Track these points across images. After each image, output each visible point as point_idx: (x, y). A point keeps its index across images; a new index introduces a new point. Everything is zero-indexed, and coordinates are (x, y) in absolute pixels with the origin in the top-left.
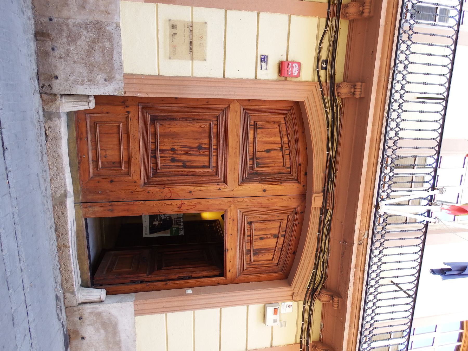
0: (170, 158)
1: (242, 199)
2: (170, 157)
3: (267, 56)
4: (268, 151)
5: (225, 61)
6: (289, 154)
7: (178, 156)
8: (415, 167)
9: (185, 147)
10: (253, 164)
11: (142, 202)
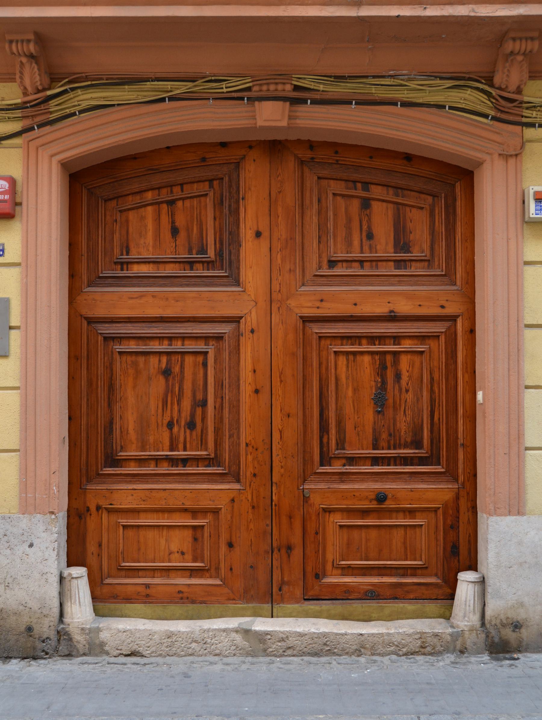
0: (188, 431)
1: (274, 282)
2: (185, 432)
4: (175, 231)
6: (182, 185)
7: (183, 415)
9: (165, 403)
10: (203, 262)
11: (274, 488)
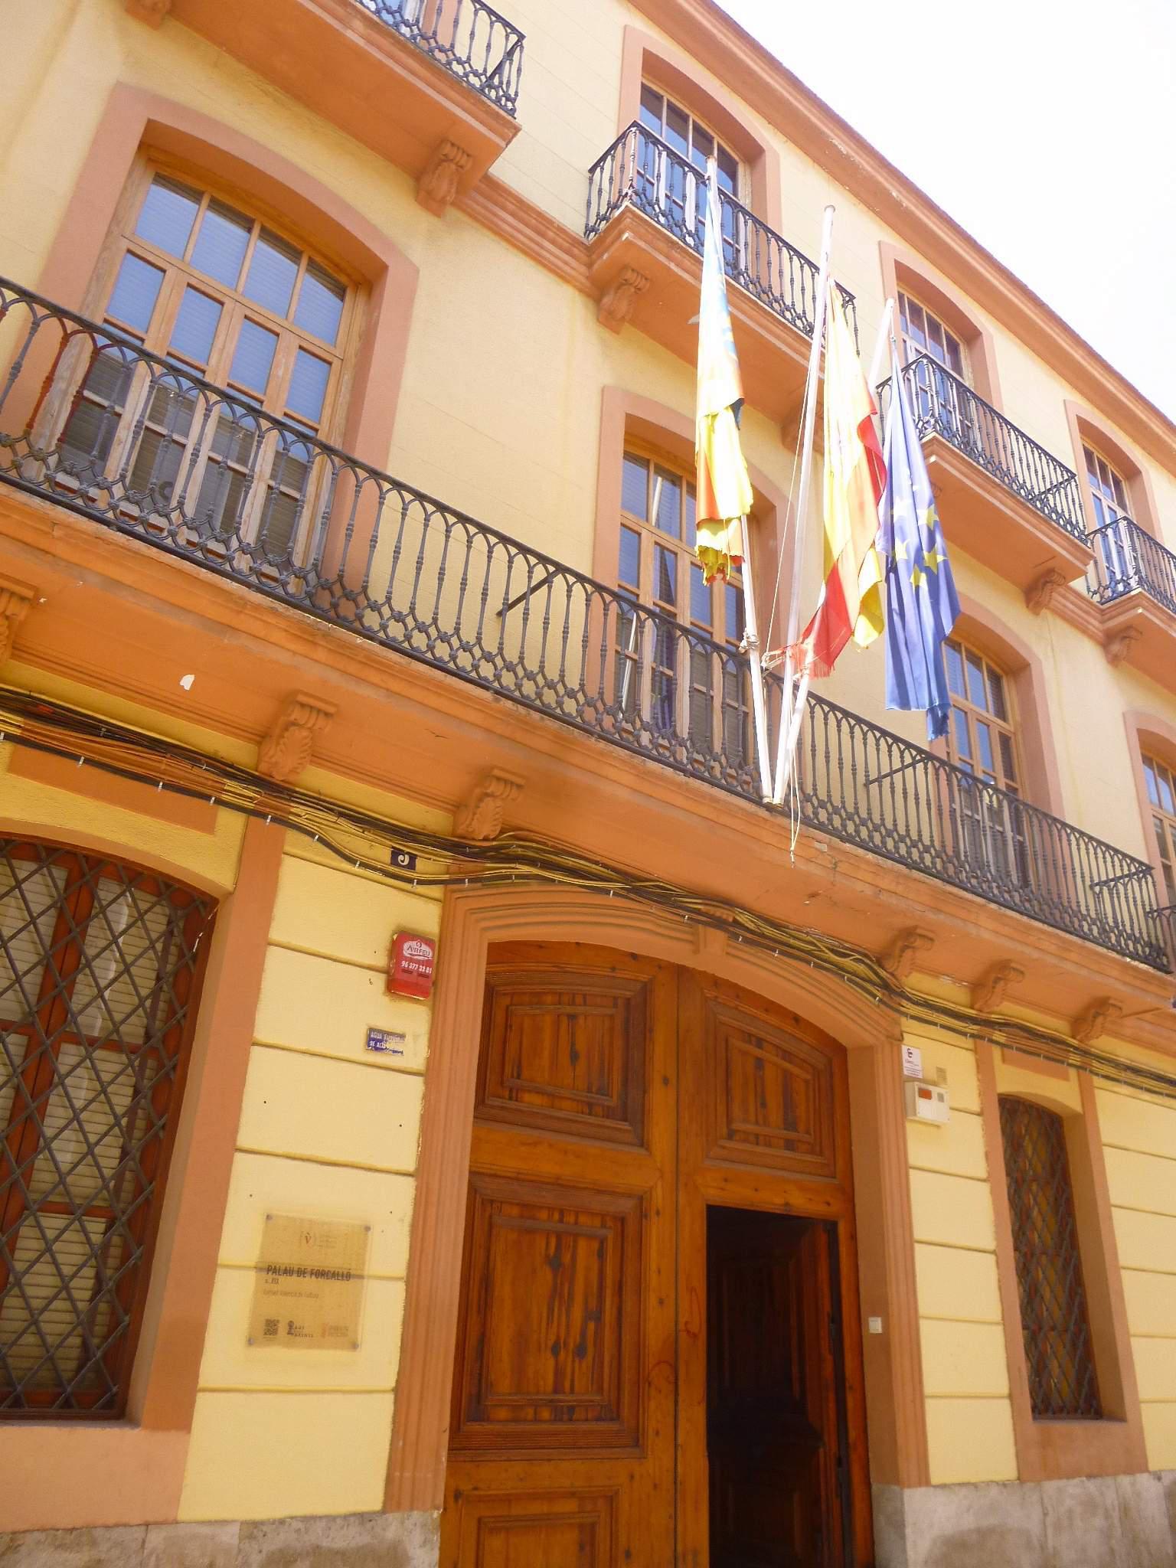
3: (371, 1030)
4: (574, 1056)
5: (370, 1169)
8: (118, 409)
9: (551, 1310)
